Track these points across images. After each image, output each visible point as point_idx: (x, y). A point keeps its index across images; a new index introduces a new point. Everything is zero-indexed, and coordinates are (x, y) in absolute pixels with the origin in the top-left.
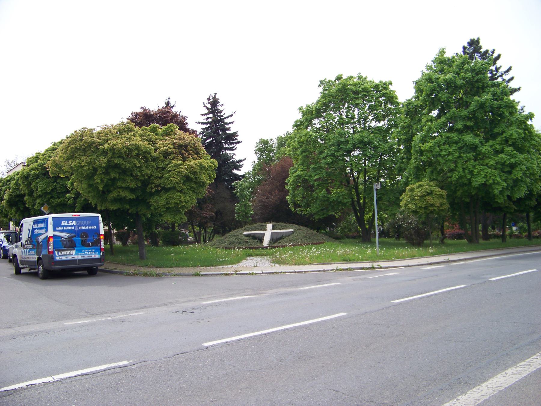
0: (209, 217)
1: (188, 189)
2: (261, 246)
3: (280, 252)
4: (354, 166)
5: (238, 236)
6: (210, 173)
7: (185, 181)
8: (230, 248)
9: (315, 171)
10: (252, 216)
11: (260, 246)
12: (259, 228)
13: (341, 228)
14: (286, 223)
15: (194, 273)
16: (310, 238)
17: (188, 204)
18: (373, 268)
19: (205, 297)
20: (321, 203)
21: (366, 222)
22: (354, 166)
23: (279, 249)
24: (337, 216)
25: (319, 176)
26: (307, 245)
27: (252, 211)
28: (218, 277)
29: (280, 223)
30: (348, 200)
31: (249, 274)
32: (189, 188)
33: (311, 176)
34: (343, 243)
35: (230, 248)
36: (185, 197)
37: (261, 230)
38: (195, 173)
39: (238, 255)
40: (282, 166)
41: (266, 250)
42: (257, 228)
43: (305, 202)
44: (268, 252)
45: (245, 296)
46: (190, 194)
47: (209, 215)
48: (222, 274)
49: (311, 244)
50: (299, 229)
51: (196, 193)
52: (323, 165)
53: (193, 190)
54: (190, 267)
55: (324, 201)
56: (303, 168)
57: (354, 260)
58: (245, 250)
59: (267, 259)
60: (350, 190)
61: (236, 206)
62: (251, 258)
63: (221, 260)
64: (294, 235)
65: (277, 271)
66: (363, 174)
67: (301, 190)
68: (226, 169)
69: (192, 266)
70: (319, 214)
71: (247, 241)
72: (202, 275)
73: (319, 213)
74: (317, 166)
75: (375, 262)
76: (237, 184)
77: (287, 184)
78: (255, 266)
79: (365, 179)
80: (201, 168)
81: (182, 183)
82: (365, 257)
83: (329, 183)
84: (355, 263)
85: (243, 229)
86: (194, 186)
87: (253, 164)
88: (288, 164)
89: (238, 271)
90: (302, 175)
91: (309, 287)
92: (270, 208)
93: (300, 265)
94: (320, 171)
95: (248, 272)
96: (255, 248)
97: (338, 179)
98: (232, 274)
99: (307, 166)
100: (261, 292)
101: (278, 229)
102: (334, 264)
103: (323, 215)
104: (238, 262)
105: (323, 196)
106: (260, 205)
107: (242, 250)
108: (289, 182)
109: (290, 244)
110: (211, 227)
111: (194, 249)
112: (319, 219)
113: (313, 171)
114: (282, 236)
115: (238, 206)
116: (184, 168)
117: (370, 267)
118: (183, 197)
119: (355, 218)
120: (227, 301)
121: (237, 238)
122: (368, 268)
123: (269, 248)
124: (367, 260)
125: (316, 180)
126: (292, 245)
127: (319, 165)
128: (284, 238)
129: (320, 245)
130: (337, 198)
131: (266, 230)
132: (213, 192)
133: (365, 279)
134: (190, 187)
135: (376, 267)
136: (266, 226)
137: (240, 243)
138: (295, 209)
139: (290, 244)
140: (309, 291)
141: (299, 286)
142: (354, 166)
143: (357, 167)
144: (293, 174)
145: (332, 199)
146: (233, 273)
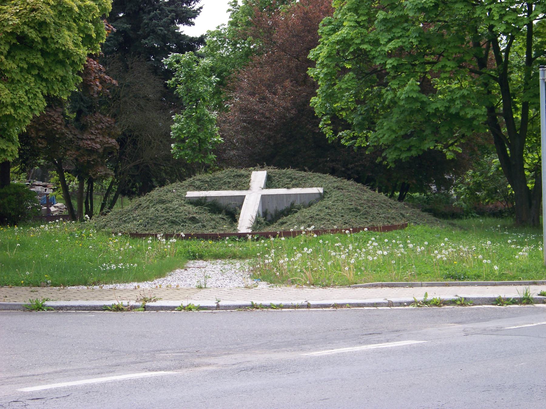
0: (101, 151)
1: (22, 70)
2: (231, 231)
3: (277, 249)
4: (496, 18)
5: (171, 202)
6: (86, 27)
7: (13, 47)
8: (145, 235)
9: (389, 30)
10: (218, 150)
11: (227, 232)
12: (229, 183)
13: (468, 188)
14: (305, 171)
15: (28, 302)
16: (366, 213)
17: (20, 111)
18: (527, 300)
19: (39, 371)
20: (402, 116)
21: (527, 173)
22: (496, 18)
23: (276, 240)
24: (449, 156)
25: (400, 44)
26: (356, 230)
27: (217, 136)
28: (92, 315)
29: (290, 171)
30: (477, 112)
31: (182, 308)
32: (26, 66)
33: (376, 43)
34: (461, 228)
35: (145, 235)
36: (13, 91)
37: (235, 188)
38: (41, 25)
39: (163, 257)
40: (306, 13)
41: (243, 243)
42: (225, 183)
43: (361, 114)
44: (248, 249)
45: (149, 370)
46: (27, 84)
47: (101, 142)
48: (104, 308)
49: (366, 229)
50: (338, 188)
51: (46, 80)
52: (411, 14)
53: (36, 72)
54: (22, 285)
55: (412, 112)
56: (356, 22)
57: (478, 277)
58: (185, 242)
59: (242, 269)
60: (486, 85)
61: (173, 122)
62: (200, 263)
63: (113, 266)
64: (323, 203)
65: (257, 302)
66: (523, 39)
67: (349, 80)
68: (151, 19)
69: (28, 284)
70: (396, 148)
71: (194, 218)
72: (49, 309)
73: (398, 146)
74: (396, 14)
75: (535, 284)
76: (178, 62)
77: (312, 64)
78: (200, 288)
79: (529, 53)
80: (60, 12)
81: (5, 52)
82: (509, 269)
83: (429, 63)
84: (479, 285)
85: (186, 183)
86: (40, 61)
87: (231, 8)
88: (320, 11)
89: (150, 300)
90: (352, 39)
91: (336, 351)
92: (270, 130)
93: (327, 286)
94: (404, 29)
95: (177, 303)
96: (215, 237)
97: (450, 51)
98: (132, 308)
99: (367, 14)
100: (197, 361)
101: (283, 187)
102: (422, 285)
103: (409, 150)
104: (161, 274)
105: (408, 99)
106: (244, 121)
107: (175, 240)
108: (317, 57)
109: (310, 229)
110: (106, 176)
111: (48, 237)
112: (398, 161)
113: (383, 28)
114: (292, 204)
115: (178, 121)
116: (13, 10)
117: (518, 296)
118: (7, 91)
119: (498, 159)
120: (93, 386)
121: (166, 209)
122: (514, 299)
123: (250, 237)
124: (514, 278)
125: (389, 55)
126: (316, 232)
127: (401, 13)
128: (296, 212)
129: (393, 233)
130: (447, 105)
131: (248, 189)
132: (114, 82)
133: (498, 330)
134: (28, 63)
135: (535, 296)
136: (248, 176)
137: (173, 222)
138: (335, 133)
139: (310, 229)
140: (329, 361)
141: (308, 347)
142: (495, 18)
143: (506, 19)
144: (329, 35)
145: (434, 106)
146: (137, 304)
